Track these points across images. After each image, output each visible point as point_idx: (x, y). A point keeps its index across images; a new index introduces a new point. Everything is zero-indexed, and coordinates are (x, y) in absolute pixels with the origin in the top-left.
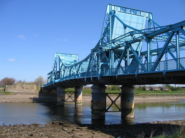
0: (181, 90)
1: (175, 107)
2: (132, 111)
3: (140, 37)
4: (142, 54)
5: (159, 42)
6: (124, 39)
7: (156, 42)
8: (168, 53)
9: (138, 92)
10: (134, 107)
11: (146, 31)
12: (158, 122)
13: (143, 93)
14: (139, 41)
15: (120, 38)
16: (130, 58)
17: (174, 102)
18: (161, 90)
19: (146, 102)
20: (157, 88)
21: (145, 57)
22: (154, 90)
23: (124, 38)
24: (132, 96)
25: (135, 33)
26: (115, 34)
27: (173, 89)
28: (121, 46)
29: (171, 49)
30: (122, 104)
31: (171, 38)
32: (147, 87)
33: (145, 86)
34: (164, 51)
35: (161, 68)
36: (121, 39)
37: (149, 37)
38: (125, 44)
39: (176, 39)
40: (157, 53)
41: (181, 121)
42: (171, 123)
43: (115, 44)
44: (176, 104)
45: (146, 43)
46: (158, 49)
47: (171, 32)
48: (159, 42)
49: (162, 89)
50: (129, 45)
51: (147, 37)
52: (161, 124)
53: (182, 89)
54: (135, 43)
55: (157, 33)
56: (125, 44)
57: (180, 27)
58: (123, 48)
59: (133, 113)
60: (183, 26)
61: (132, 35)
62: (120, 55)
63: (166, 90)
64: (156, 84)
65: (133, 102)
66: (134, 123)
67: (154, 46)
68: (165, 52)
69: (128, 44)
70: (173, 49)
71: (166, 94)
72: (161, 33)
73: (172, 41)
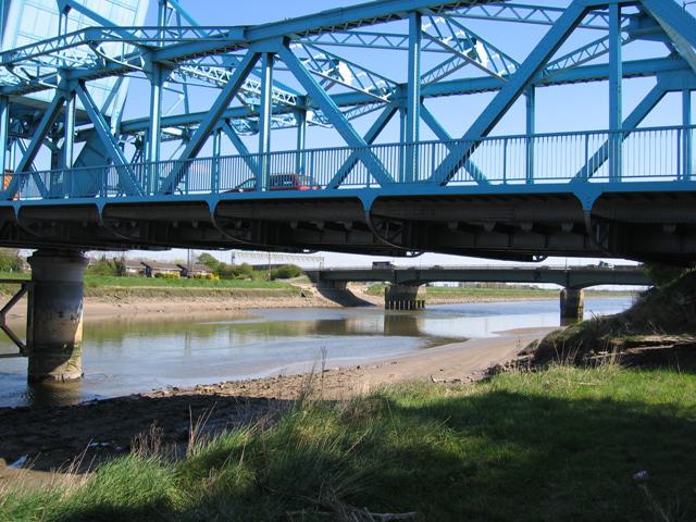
0: (251, 277)
1: (228, 334)
2: (75, 353)
3: (127, 57)
4: (125, 129)
5: (199, 89)
6: (55, 54)
7: (180, 88)
8: (222, 133)
9: (97, 281)
10: (80, 339)
11: (152, 34)
12: (175, 389)
13: (117, 284)
14: (120, 72)
15: (41, 47)
16: (78, 138)
17: (226, 319)
18: (183, 274)
19: (126, 319)
20: (169, 265)
21: (134, 140)
22: (157, 276)
23: (58, 50)
24: (74, 292)
25: (109, 35)
26: (18, 33)
27: (226, 273)
28: (41, 82)
29: (233, 122)
30: (32, 325)
31: (242, 80)
32: (132, 263)
33: (123, 258)
34: (214, 123)
35: (197, 184)
36: (47, 53)
37: (160, 63)
38: (59, 78)
39: (262, 89)
40: (184, 130)
41: (254, 384)
42: (223, 393)
43: (14, 70)
44: (232, 326)
45: (148, 82)
46: (188, 115)
47: (244, 52)
48: (199, 89)
49: (184, 271)
50: (75, 85)
51: (153, 63)
52: (186, 397)
53: (257, 273)
54: (98, 81)
55: (191, 50)
56: (59, 78)
57: (282, 40)
58: (48, 96)
59: (79, 359)
60: (293, 36)
61: (94, 45)
62: (34, 122)
63: (200, 277)
64: (174, 250)
65: (78, 316)
66: (84, 398)
67: (173, 106)
68: (215, 129)
69: (73, 81)
70: (243, 121)
71: (201, 288)
72: (210, 53)
73: (243, 90)
